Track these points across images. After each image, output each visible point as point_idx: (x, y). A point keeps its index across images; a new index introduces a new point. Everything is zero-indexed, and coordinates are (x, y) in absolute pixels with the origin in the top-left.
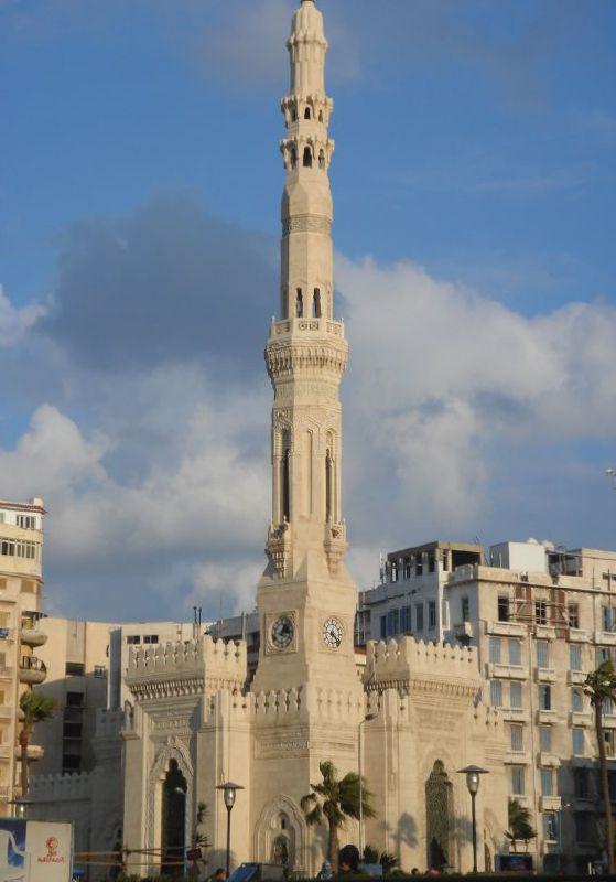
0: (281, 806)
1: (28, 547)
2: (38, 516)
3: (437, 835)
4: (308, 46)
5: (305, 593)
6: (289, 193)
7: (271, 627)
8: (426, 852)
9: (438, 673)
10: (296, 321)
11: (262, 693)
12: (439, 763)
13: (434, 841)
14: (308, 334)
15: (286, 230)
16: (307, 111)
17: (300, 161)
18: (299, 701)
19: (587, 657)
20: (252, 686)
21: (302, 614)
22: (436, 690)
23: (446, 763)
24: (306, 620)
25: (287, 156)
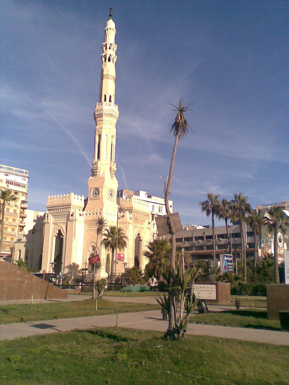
2: (27, 179)
3: (137, 254)
5: (104, 181)
6: (103, 68)
7: (92, 192)
10: (104, 103)
11: (89, 211)
15: (102, 79)
16: (110, 47)
17: (107, 60)
18: (100, 213)
20: (85, 209)
25: (103, 59)
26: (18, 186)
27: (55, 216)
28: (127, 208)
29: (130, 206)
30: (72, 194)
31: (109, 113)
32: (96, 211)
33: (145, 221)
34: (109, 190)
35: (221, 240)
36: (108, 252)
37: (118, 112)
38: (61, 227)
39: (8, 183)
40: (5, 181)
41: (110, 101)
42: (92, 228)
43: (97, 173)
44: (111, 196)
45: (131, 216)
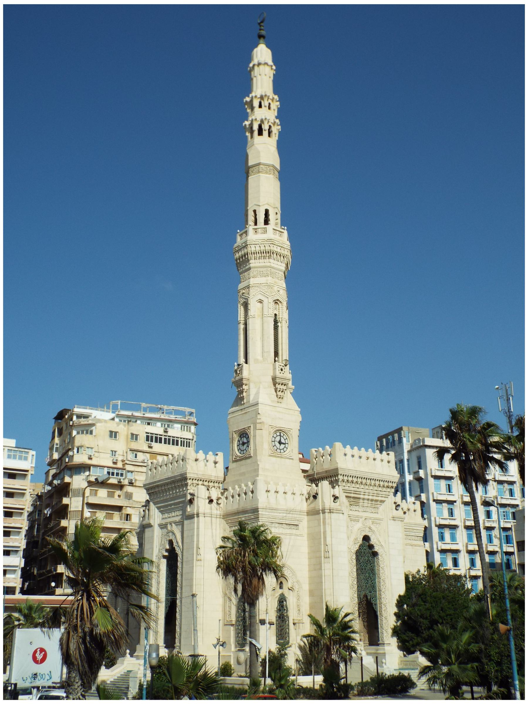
1: (187, 442)
9: (362, 469)
12: (366, 538)
13: (366, 596)
14: (260, 236)
16: (260, 103)
17: (256, 133)
18: (252, 492)
19: (492, 487)
21: (255, 428)
22: (361, 483)
26: (173, 444)
29: (333, 467)
30: (338, 445)
34: (272, 431)
36: (280, 591)
39: (152, 441)
40: (142, 437)
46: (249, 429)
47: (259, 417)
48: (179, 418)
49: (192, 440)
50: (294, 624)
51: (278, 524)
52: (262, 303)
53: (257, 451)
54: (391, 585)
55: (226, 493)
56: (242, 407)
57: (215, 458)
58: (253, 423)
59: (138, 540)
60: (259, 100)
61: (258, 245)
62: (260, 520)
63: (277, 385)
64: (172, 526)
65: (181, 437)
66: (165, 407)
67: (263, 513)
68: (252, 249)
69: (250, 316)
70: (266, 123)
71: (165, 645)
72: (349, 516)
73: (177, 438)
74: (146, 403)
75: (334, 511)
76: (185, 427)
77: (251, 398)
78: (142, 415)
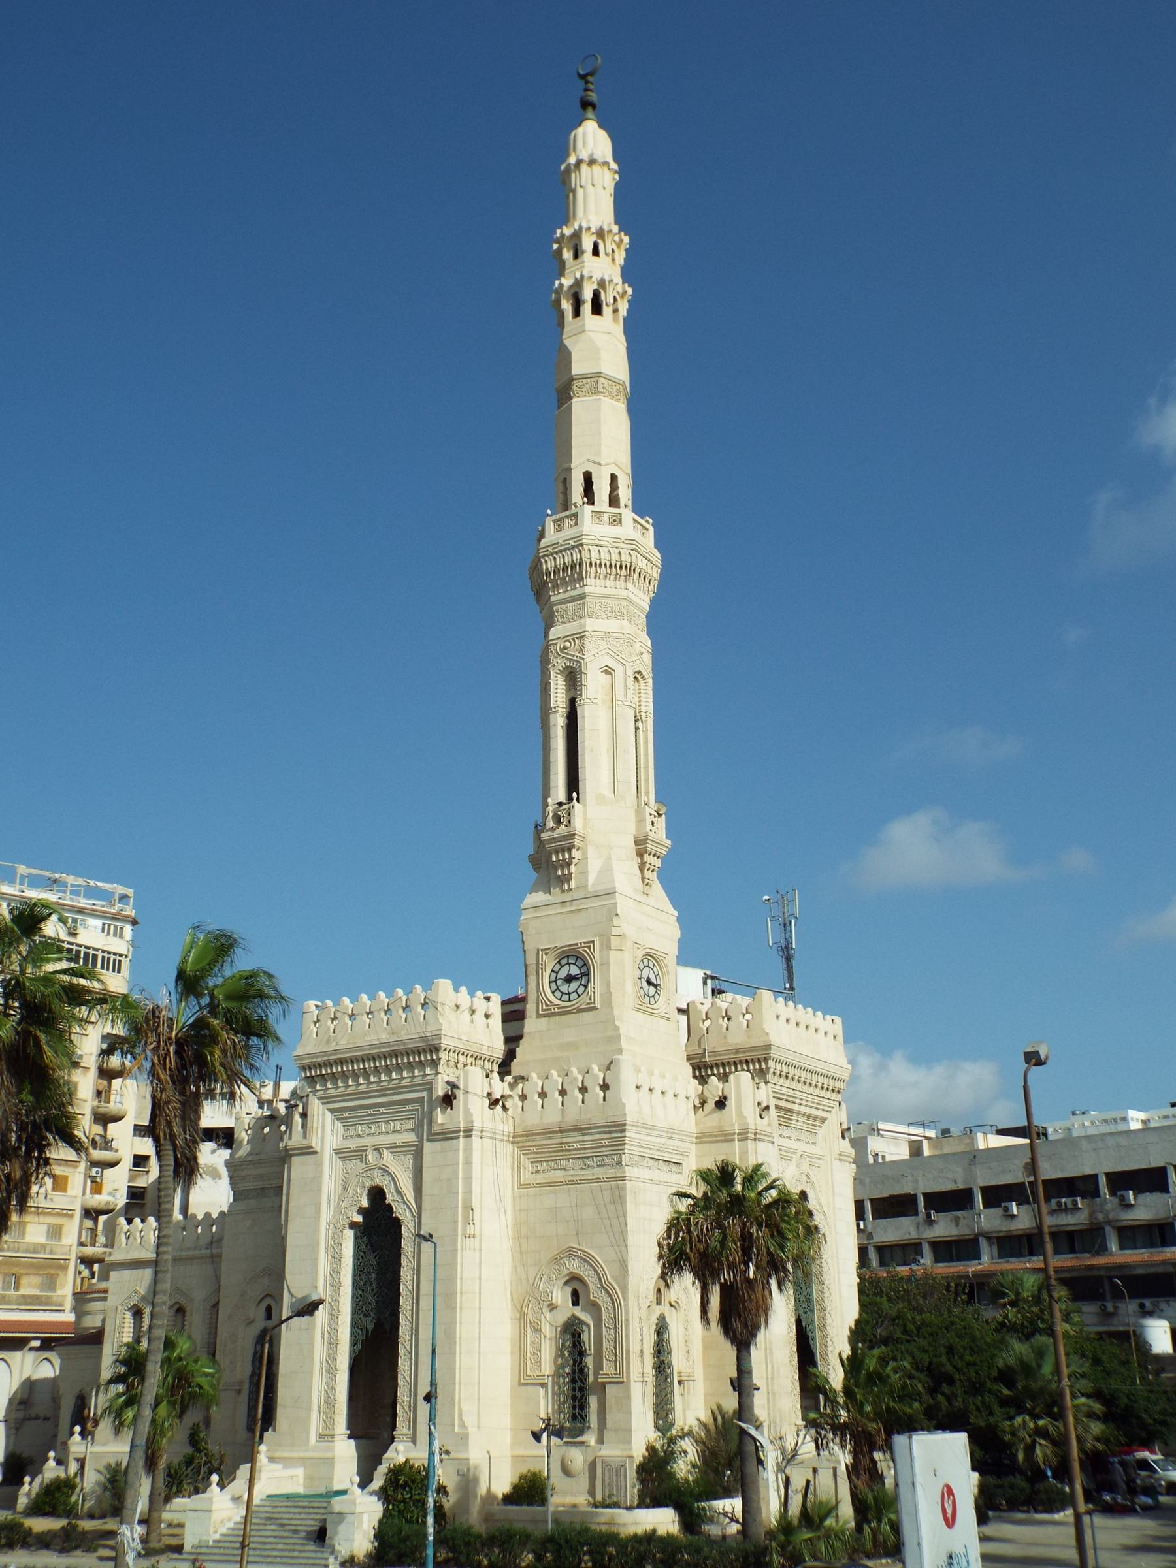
0: (575, 1267)
1: (115, 960)
4: (596, 168)
5: (613, 913)
7: (549, 970)
8: (797, 1384)
14: (606, 531)
17: (587, 308)
18: (605, 1087)
21: (607, 946)
23: (811, 1196)
24: (613, 955)
27: (346, 1114)
28: (737, 1051)
30: (444, 986)
31: (605, 557)
32: (580, 1078)
33: (823, 1120)
34: (640, 953)
35: (1080, 1206)
37: (656, 556)
38: (385, 1170)
41: (614, 501)
42: (558, 1175)
43: (573, 869)
44: (652, 989)
45: (764, 1094)
46: (589, 947)
47: (616, 922)
48: (100, 905)
49: (126, 956)
50: (680, 1382)
51: (651, 1161)
52: (611, 674)
53: (613, 998)
54: (840, 1296)
55: (520, 1086)
56: (567, 897)
57: (488, 1007)
58: (601, 935)
59: (231, 1184)
60: (594, 238)
61: (606, 550)
62: (626, 1151)
63: (646, 855)
64: (380, 1154)
65: (105, 948)
66: (70, 879)
67: (633, 1135)
68: (602, 557)
69: (587, 701)
70: (610, 289)
71: (348, 1432)
72: (780, 1150)
73: (95, 949)
74: (29, 866)
75: (762, 1137)
76: (112, 927)
77: (591, 879)
78: (18, 893)
